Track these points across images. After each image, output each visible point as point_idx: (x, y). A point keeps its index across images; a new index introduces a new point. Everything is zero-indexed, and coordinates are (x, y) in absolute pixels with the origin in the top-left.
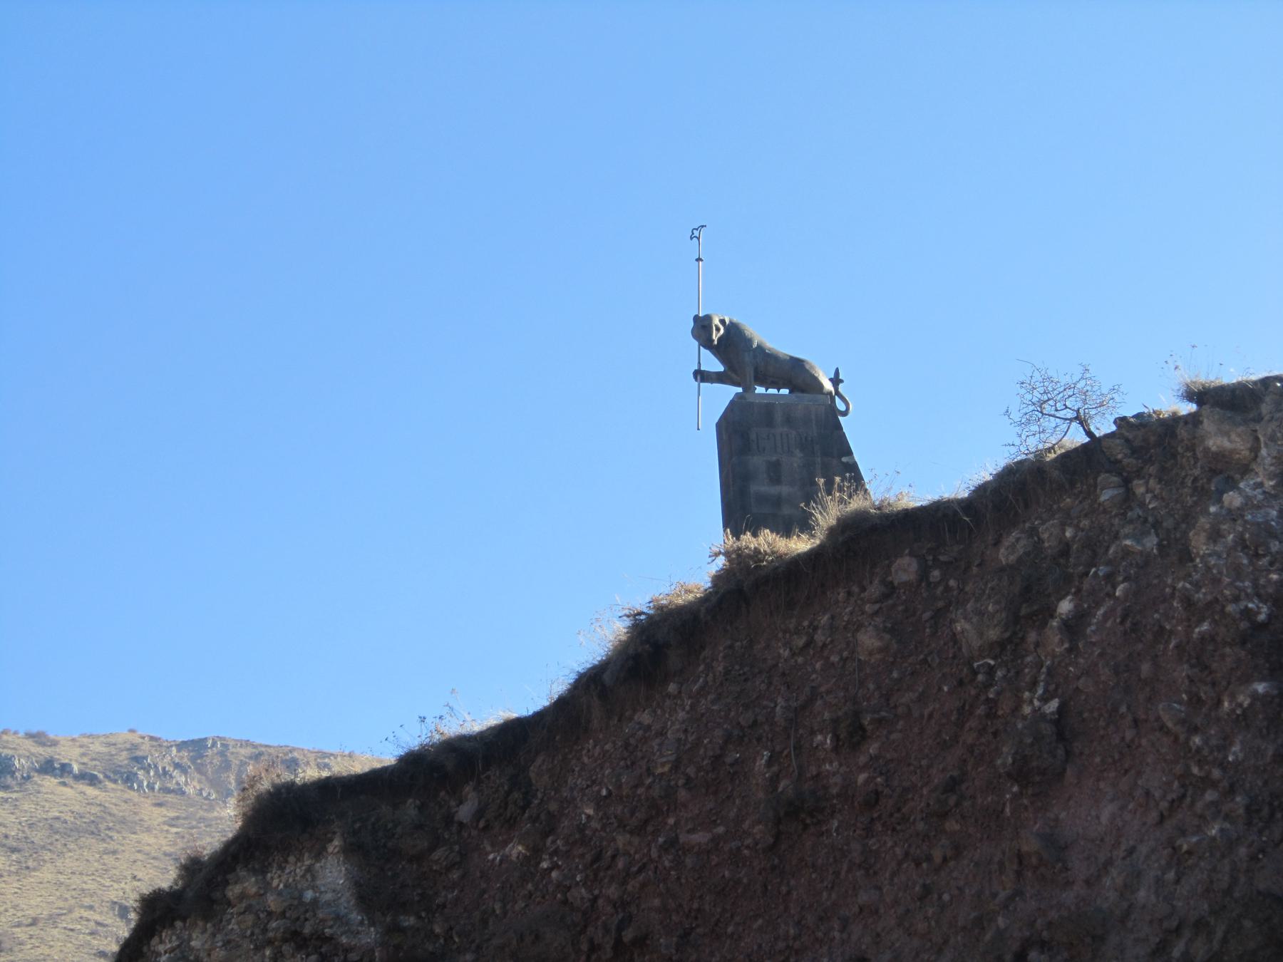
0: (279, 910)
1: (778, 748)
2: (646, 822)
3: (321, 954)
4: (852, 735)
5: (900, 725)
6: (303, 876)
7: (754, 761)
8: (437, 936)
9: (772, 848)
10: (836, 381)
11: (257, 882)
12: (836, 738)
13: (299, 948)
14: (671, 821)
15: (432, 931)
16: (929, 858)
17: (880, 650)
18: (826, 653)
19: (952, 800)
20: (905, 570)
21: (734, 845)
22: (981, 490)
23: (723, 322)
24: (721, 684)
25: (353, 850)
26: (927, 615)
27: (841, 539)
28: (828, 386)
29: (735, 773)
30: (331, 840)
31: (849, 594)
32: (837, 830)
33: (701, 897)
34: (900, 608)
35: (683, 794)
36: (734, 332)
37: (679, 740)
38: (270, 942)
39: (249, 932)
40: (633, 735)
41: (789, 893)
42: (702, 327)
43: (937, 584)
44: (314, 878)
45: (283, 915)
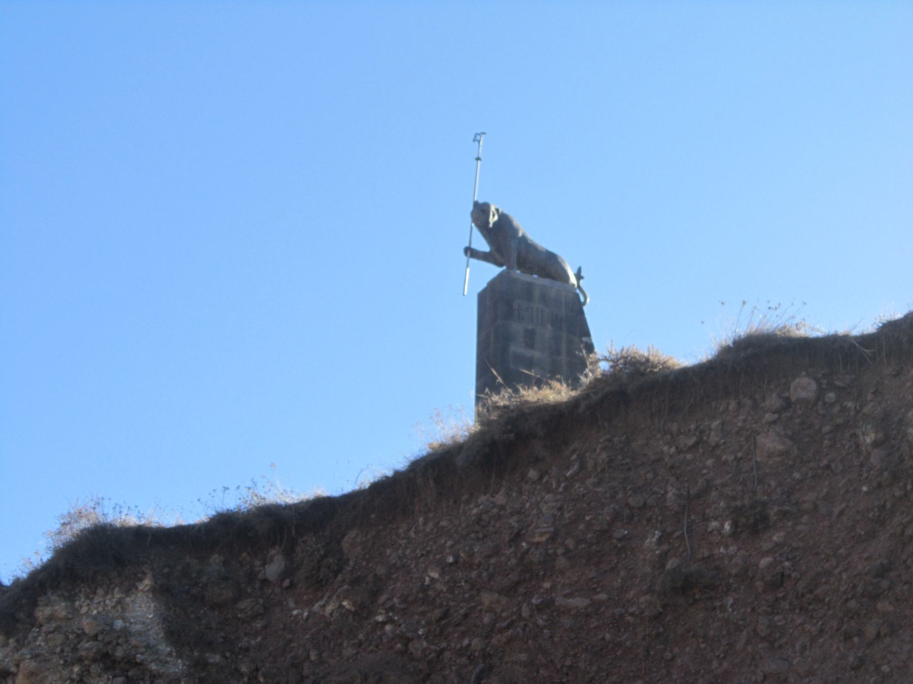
0: (92, 633)
1: (669, 530)
2: (517, 584)
3: (127, 677)
4: (752, 524)
5: (805, 519)
6: (114, 607)
7: (644, 538)
8: (242, 675)
9: (658, 617)
10: (579, 277)
11: (67, 607)
12: (735, 524)
13: (106, 669)
14: (547, 585)
15: (237, 670)
16: (860, 633)
17: (781, 454)
18: (718, 452)
19: (885, 584)
20: (804, 389)
21: (618, 611)
22: (397, 473)
23: (497, 210)
24: (603, 471)
25: (162, 591)
26: (827, 429)
27: (743, 354)
28: (573, 280)
29: (622, 547)
30: (141, 580)
31: (740, 405)
32: (732, 606)
33: (575, 656)
34: (797, 421)
35: (561, 562)
36: (504, 220)
37: (554, 516)
38: (80, 660)
39: (58, 650)
40: (487, 512)
41: (673, 659)
42: (480, 211)
43: (833, 405)
44: (123, 609)
45: (95, 638)
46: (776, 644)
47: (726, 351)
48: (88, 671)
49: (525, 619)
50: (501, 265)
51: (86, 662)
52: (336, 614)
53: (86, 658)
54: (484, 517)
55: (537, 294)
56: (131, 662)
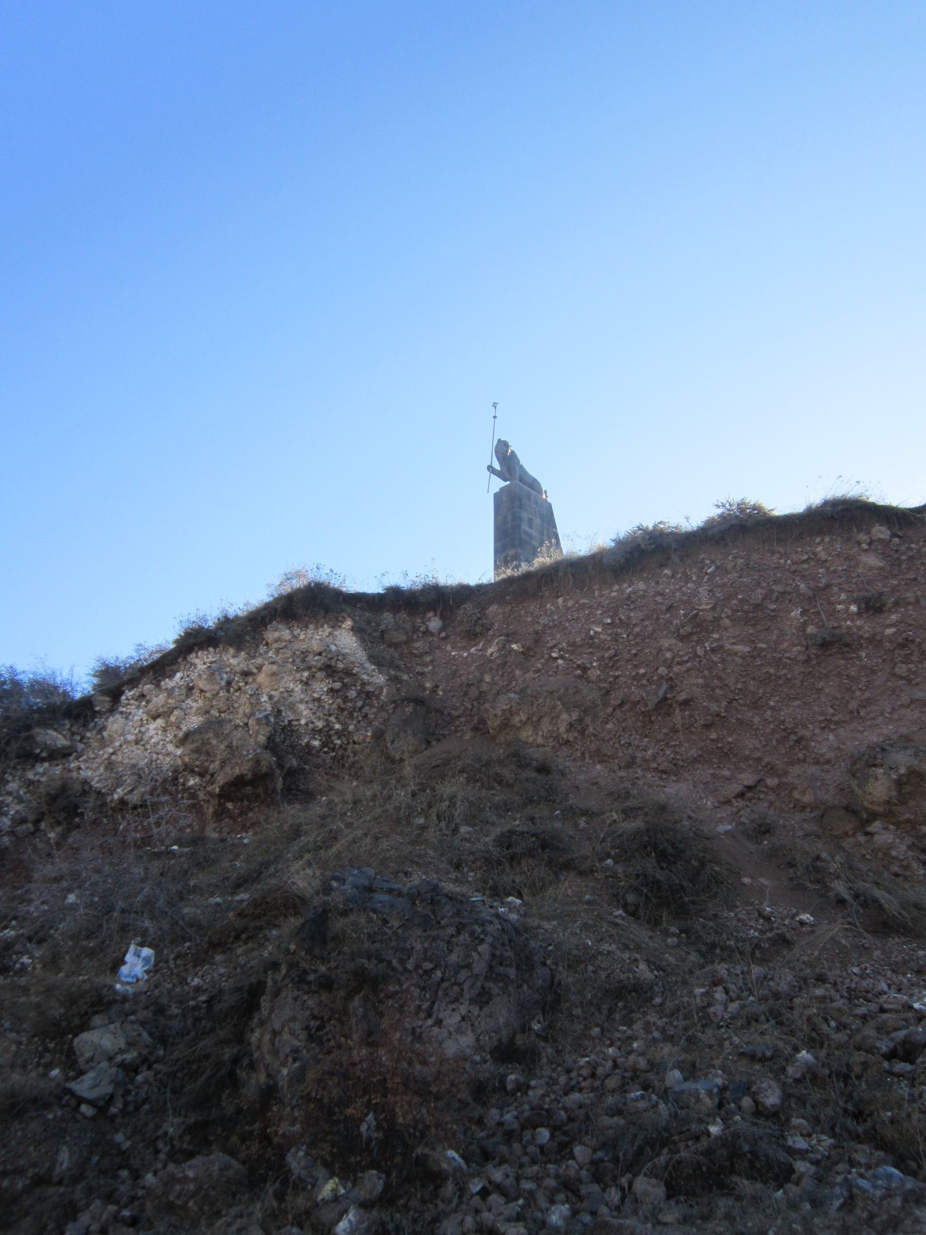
0: (319, 650)
4: (872, 607)
13: (328, 676)
17: (881, 568)
24: (742, 569)
30: (343, 622)
38: (309, 668)
39: (291, 660)
45: (320, 654)
46: (913, 682)
47: (826, 503)
48: (314, 676)
49: (700, 657)
50: (505, 480)
51: (314, 670)
52: (495, 655)
53: (315, 667)
54: (632, 596)
55: (532, 498)
56: (348, 673)
